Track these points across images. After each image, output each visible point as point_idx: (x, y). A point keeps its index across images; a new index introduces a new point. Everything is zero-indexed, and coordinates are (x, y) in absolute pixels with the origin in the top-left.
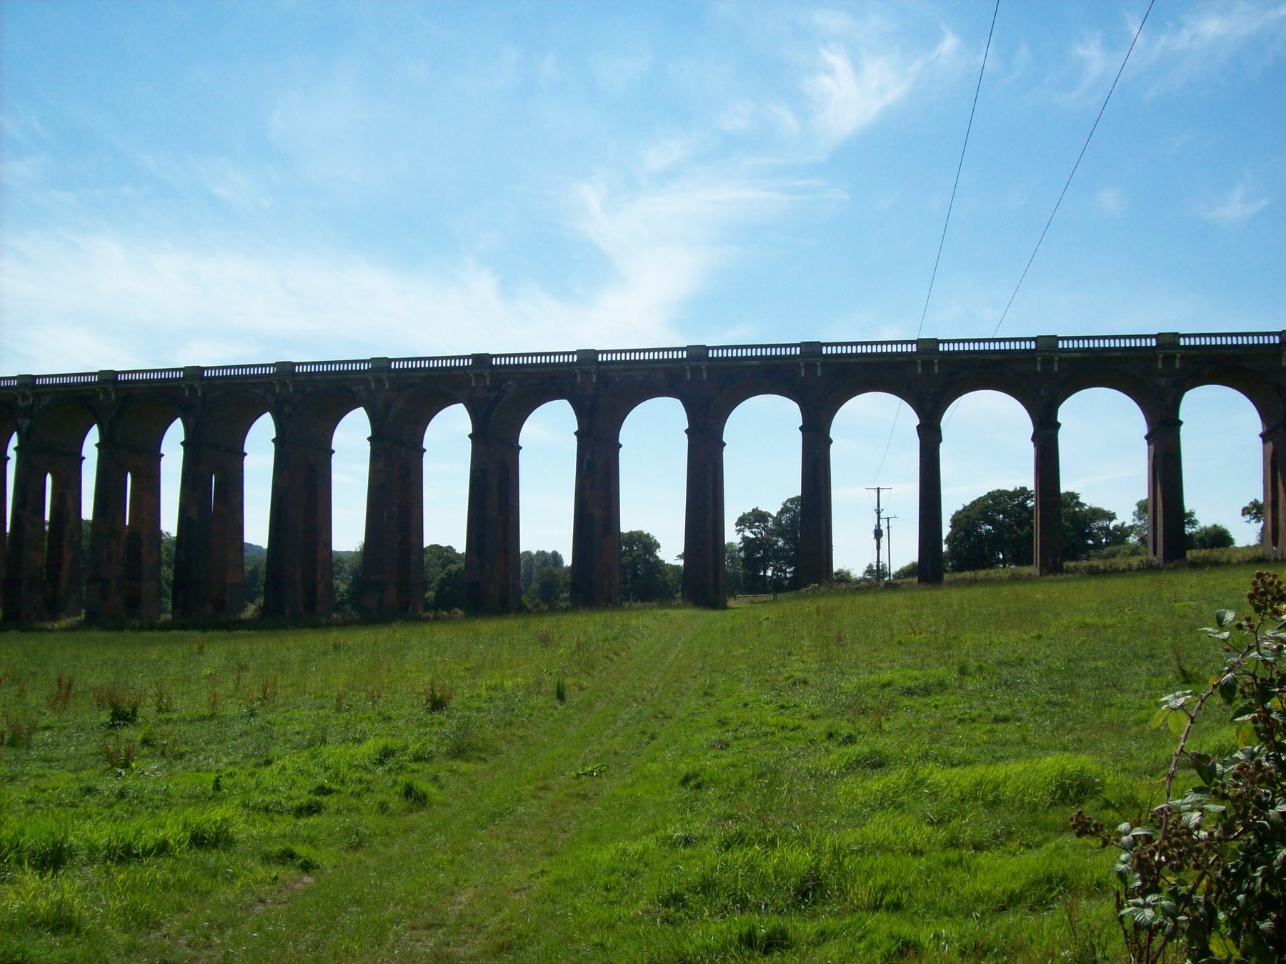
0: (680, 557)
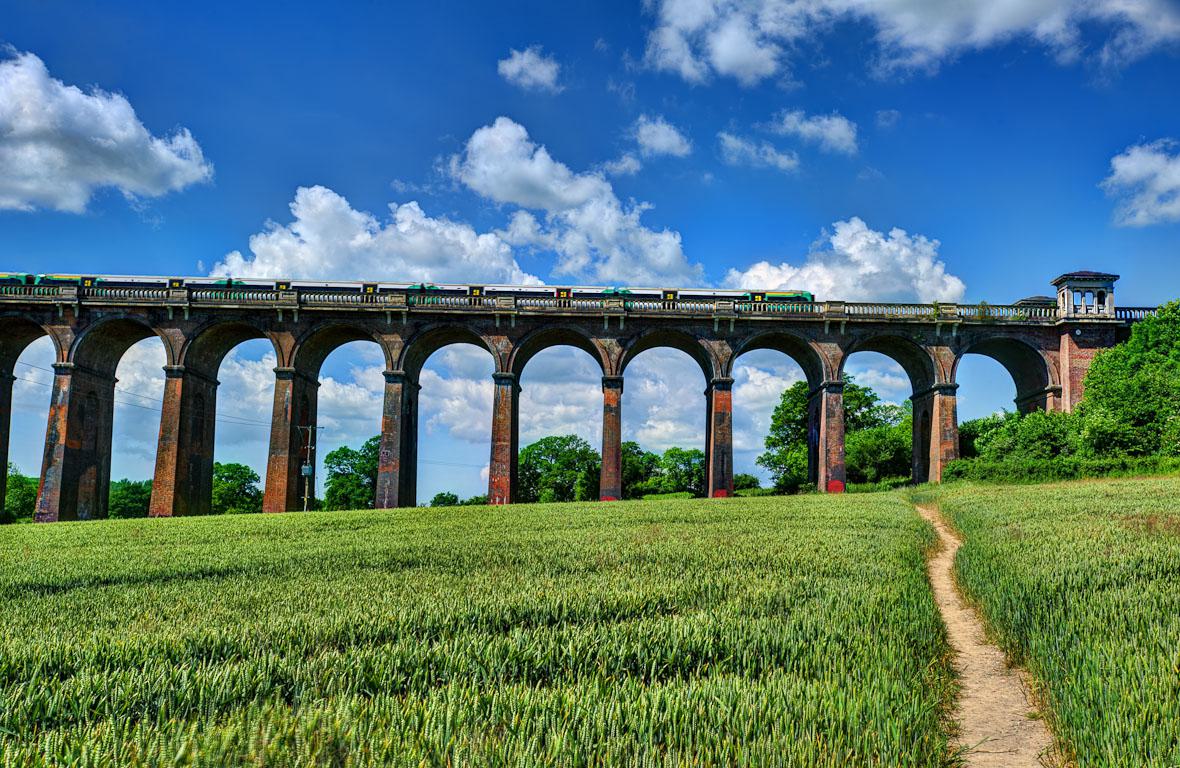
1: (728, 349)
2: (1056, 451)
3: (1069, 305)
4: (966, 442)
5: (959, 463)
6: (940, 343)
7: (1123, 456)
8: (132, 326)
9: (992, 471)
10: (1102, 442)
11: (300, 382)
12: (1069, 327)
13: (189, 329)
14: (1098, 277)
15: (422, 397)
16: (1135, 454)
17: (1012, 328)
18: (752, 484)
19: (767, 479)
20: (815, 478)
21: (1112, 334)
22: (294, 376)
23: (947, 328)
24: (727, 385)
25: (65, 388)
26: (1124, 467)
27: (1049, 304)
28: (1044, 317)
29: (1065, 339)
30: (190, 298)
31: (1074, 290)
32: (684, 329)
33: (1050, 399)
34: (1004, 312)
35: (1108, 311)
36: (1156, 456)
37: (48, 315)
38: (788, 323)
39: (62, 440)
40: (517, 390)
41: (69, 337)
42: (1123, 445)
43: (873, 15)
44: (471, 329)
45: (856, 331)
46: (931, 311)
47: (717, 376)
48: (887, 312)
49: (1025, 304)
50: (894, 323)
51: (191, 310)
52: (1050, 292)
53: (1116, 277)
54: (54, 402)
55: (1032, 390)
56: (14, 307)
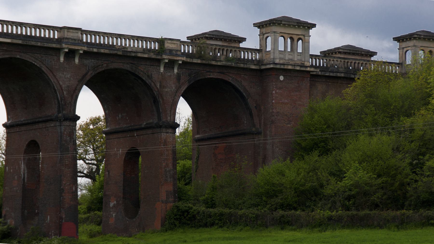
45: (90, 62)
53: (314, 26)
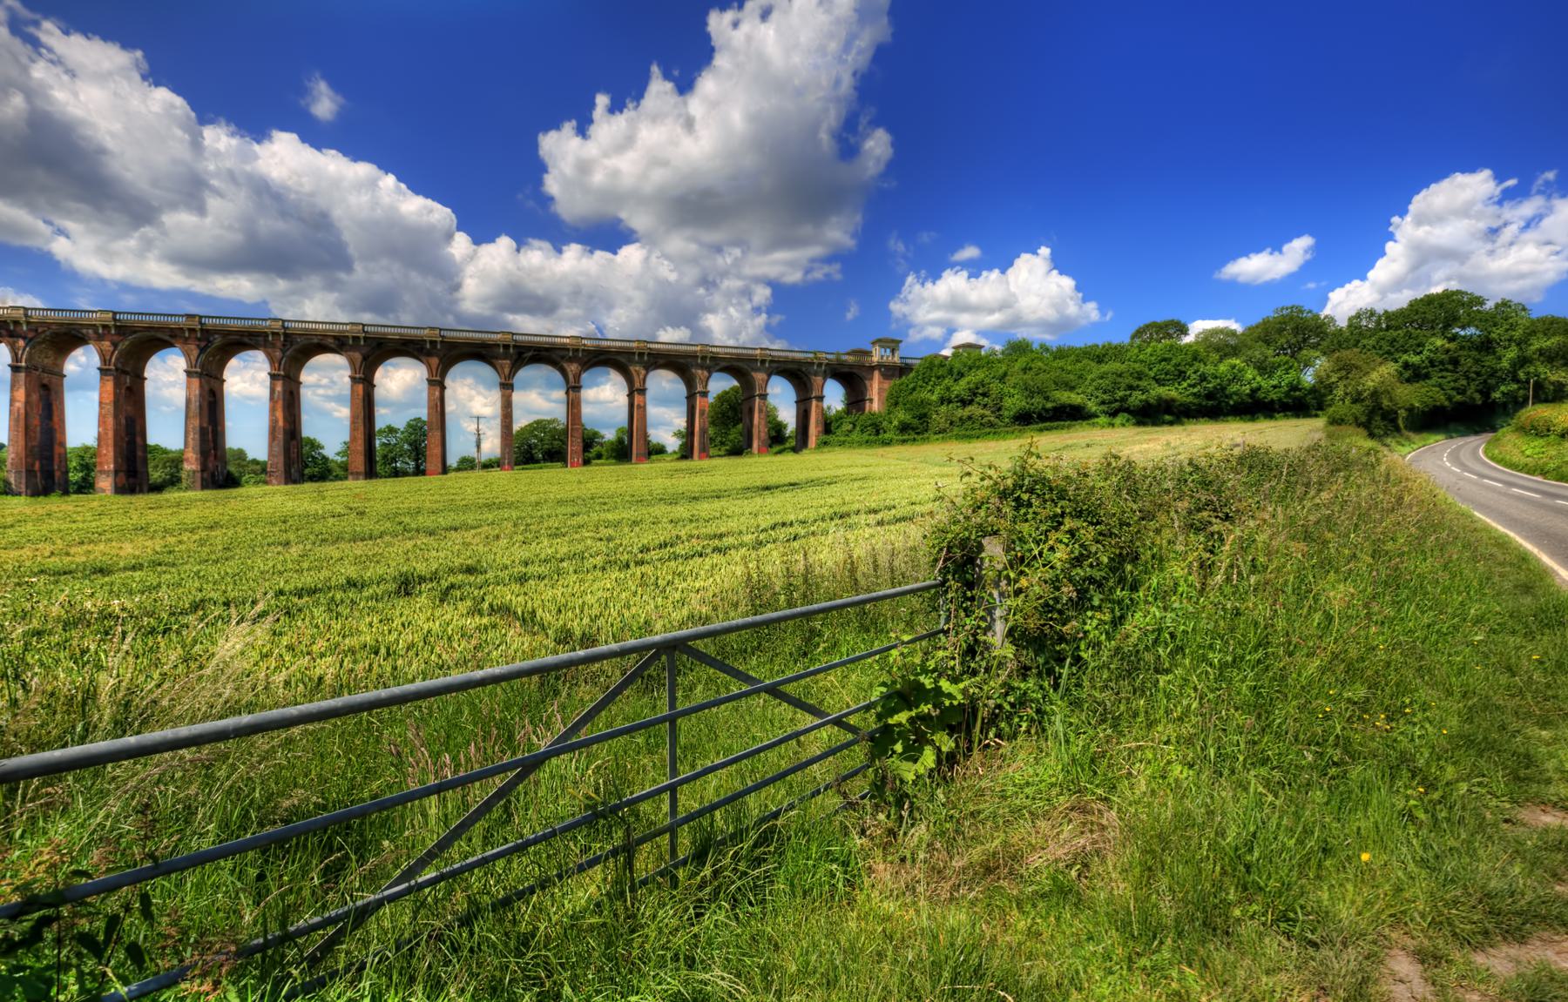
0: (338, 454)
1: (706, 373)
2: (878, 433)
3: (878, 354)
4: (828, 427)
5: (825, 438)
6: (757, 370)
7: (913, 435)
8: (67, 337)
9: (844, 442)
10: (904, 428)
11: (364, 381)
12: (879, 366)
13: (365, 350)
14: (893, 341)
15: (303, 391)
16: (918, 433)
17: (851, 366)
18: (660, 450)
19: (672, 443)
20: (750, 445)
21: (897, 373)
22: (200, 375)
23: (820, 365)
24: (643, 391)
25: (279, 388)
26: (915, 440)
27: (868, 353)
28: (867, 361)
29: (876, 374)
30: (115, 319)
31: (881, 347)
32: (682, 361)
33: (868, 404)
34: (586, 342)
35: (896, 359)
36: (926, 435)
37: (261, 339)
38: (739, 358)
39: (281, 423)
40: (443, 388)
41: (278, 354)
42: (913, 429)
43: (144, 78)
44: (554, 356)
45: (775, 365)
46: (811, 356)
47: (637, 385)
48: (790, 355)
49: (853, 353)
50: (794, 361)
51: (202, 330)
52: (867, 347)
54: (272, 398)
55: (856, 399)
56: (661, 361)
